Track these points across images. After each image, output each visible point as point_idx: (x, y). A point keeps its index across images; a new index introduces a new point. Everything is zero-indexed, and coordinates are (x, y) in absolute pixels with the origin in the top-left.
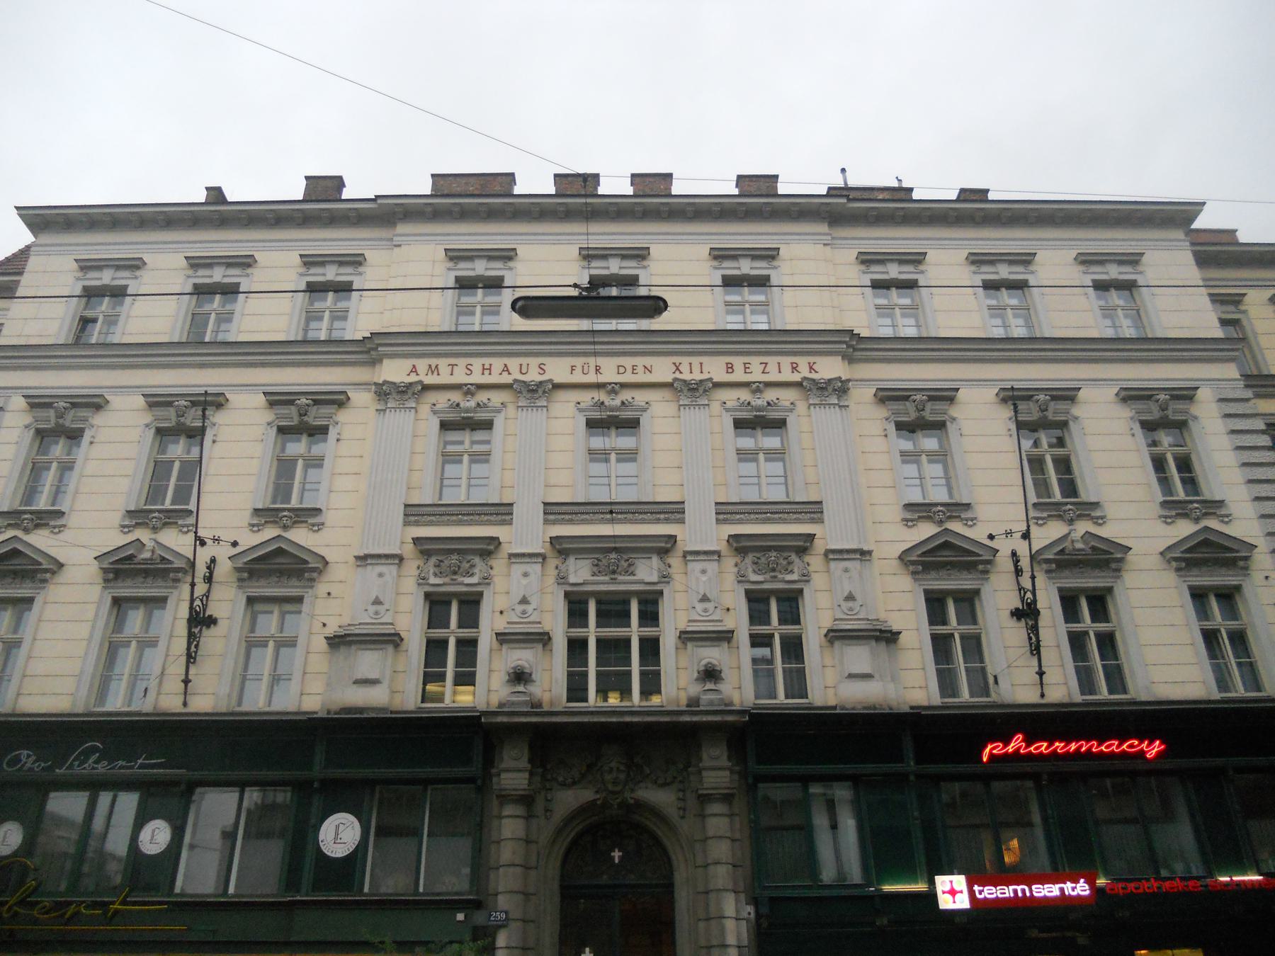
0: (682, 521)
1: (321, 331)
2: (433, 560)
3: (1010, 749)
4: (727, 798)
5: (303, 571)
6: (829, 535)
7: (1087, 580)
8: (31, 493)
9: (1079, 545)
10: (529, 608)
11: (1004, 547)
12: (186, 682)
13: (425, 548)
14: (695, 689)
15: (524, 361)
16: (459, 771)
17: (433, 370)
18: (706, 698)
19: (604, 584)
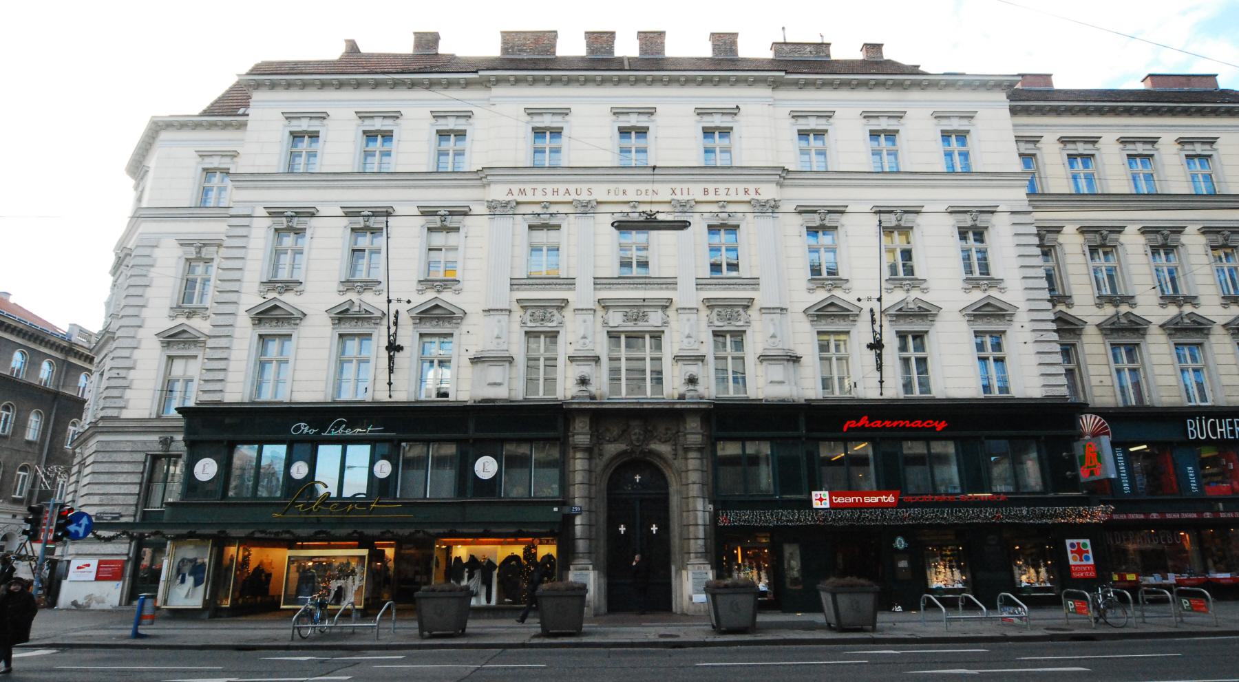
0: (676, 289)
1: (374, 164)
2: (529, 312)
3: (860, 424)
4: (700, 450)
5: (926, 316)
6: (761, 298)
7: (914, 324)
8: (276, 268)
9: (911, 306)
10: (587, 341)
11: (866, 306)
12: (390, 384)
13: (524, 305)
14: (683, 389)
15: (578, 186)
16: (551, 434)
17: (522, 192)
18: (689, 394)
19: (630, 327)
